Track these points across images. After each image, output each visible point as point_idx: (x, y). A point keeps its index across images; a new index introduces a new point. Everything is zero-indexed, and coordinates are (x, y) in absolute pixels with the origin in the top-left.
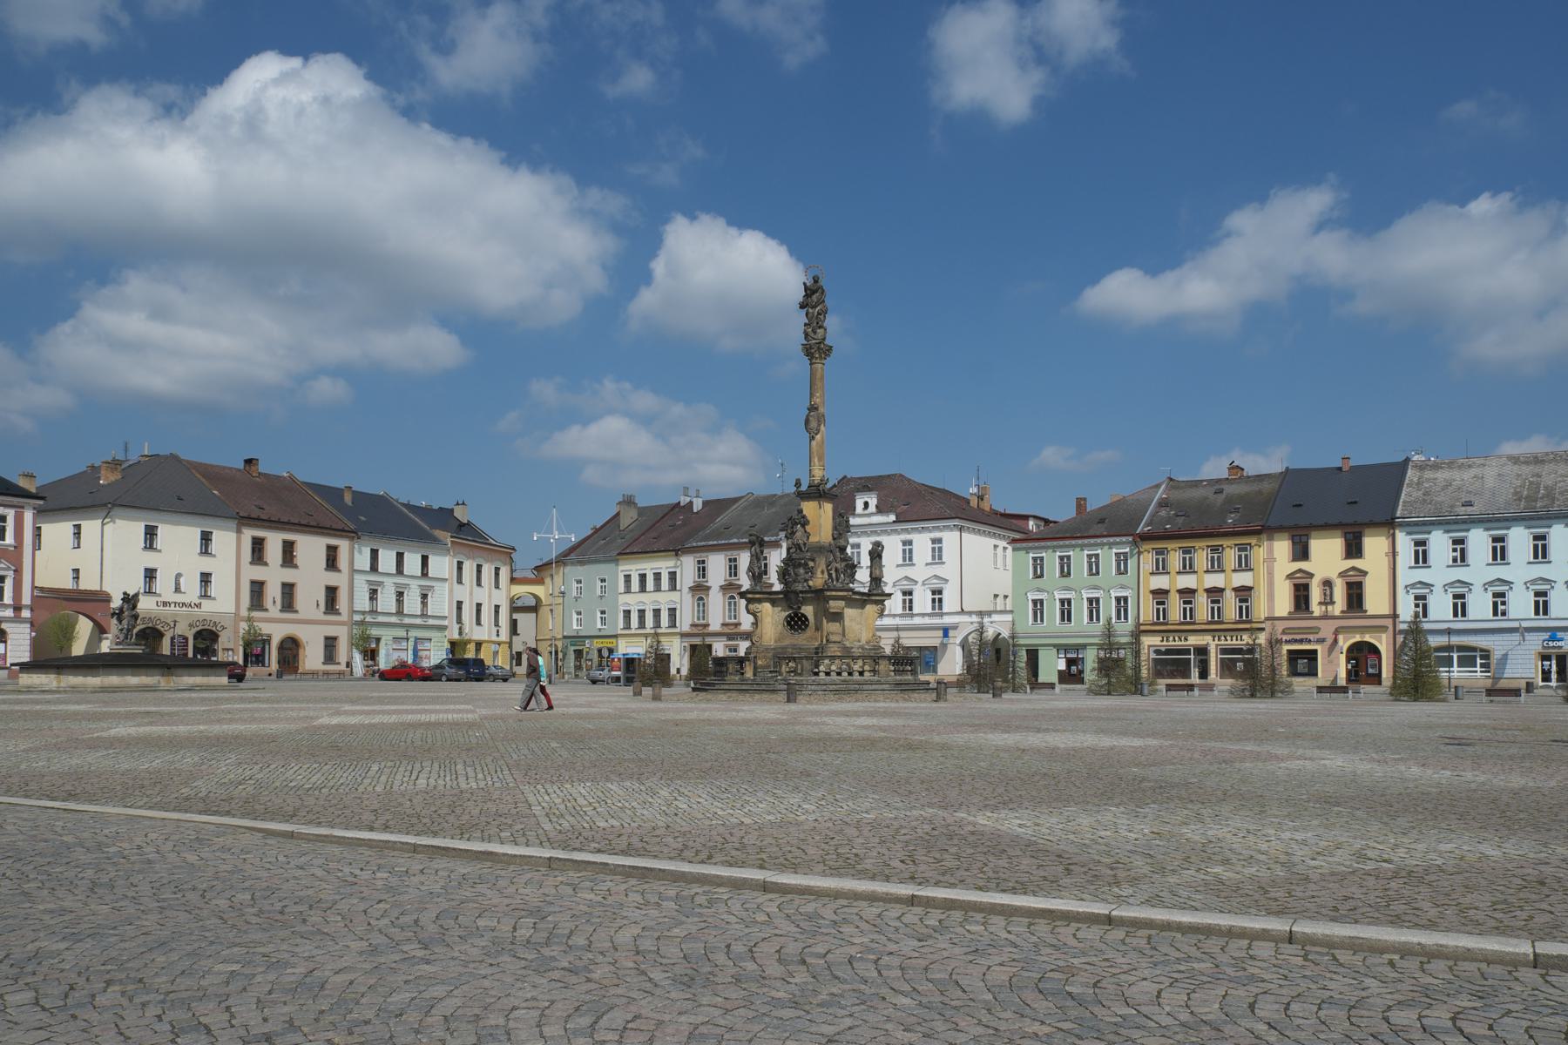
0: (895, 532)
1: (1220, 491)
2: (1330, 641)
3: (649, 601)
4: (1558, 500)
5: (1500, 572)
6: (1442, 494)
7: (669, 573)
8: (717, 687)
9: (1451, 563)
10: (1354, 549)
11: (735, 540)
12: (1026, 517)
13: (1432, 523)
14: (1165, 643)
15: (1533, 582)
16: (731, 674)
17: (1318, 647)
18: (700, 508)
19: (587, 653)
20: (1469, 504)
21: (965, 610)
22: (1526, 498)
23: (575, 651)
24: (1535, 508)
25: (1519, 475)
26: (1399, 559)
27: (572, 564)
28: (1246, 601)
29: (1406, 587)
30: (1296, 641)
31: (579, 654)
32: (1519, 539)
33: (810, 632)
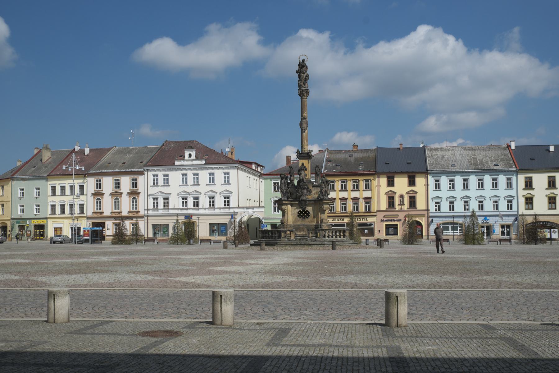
0: (206, 169)
1: (352, 156)
2: (402, 221)
3: (67, 200)
4: (486, 165)
5: (466, 193)
6: (442, 161)
7: (70, 186)
8: (278, 244)
9: (448, 189)
10: (412, 183)
11: (117, 170)
12: (251, 163)
13: (442, 173)
14: (334, 221)
15: (478, 197)
16: (283, 238)
17: (398, 223)
18: (88, 153)
19: (28, 227)
20: (453, 166)
21: (240, 206)
22: (474, 164)
23: (19, 226)
24: (478, 168)
25: (468, 155)
26: (429, 187)
27: (18, 180)
28: (369, 203)
29: (432, 198)
30: (389, 220)
31: (22, 228)
32: (473, 180)
33: (311, 218)
